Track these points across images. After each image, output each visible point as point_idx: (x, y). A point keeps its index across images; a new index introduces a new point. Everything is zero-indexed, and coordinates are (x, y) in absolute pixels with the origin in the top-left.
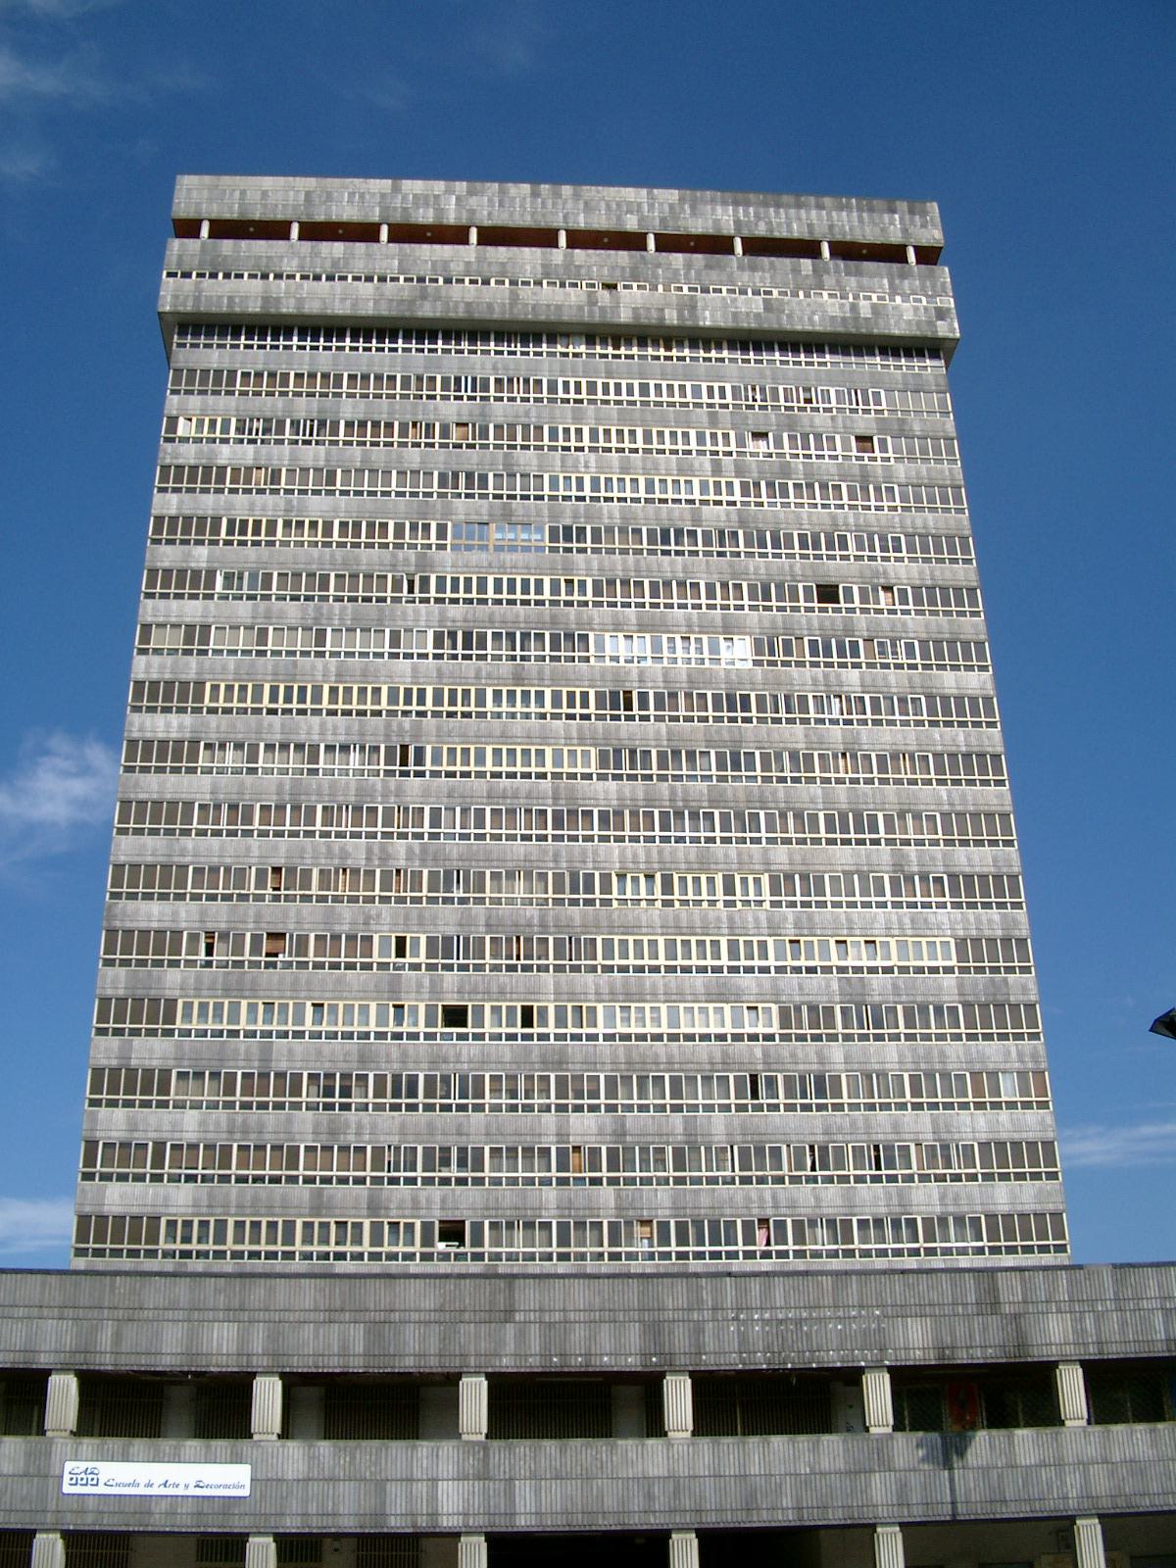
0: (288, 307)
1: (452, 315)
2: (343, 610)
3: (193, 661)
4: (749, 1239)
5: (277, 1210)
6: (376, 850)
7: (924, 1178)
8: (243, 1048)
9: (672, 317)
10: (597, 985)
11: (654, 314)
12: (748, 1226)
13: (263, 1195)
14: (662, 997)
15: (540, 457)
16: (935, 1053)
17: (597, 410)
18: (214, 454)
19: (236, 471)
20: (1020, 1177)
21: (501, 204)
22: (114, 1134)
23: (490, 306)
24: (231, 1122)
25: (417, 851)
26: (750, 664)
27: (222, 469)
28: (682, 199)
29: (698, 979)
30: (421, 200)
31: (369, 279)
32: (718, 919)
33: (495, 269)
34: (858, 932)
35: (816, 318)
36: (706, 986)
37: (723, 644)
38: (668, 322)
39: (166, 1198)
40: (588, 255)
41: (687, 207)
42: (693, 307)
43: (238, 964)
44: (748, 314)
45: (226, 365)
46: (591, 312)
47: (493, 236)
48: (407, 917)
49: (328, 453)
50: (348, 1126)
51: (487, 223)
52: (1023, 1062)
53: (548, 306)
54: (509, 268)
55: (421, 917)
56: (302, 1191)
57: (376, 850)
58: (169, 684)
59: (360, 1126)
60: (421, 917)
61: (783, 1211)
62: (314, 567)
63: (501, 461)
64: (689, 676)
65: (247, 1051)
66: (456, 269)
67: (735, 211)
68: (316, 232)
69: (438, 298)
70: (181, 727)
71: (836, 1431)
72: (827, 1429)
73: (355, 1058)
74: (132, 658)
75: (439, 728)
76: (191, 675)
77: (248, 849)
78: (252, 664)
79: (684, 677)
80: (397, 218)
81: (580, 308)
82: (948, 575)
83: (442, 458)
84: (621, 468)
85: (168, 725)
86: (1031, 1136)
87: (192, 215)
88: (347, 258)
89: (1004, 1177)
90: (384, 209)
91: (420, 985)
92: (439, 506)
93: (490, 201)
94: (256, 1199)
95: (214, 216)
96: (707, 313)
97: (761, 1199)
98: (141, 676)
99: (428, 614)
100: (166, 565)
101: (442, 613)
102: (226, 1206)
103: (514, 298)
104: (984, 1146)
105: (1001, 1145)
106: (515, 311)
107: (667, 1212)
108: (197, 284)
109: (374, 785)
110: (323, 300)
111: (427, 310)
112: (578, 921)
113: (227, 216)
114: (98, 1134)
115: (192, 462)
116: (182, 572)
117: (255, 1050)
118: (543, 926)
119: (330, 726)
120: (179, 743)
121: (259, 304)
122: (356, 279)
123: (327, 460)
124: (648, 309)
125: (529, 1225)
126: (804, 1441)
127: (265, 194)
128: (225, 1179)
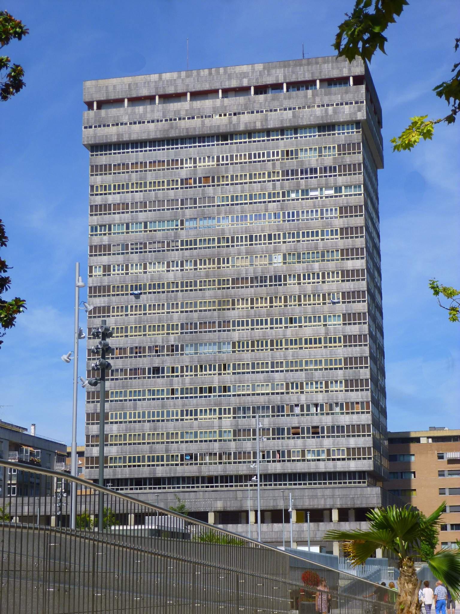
0: (126, 138)
1: (182, 134)
2: (152, 255)
3: (106, 278)
4: (274, 456)
5: (140, 453)
6: (165, 338)
7: (328, 437)
8: (128, 405)
9: (259, 126)
10: (231, 379)
11: (252, 125)
12: (274, 453)
13: (136, 448)
14: (250, 382)
15: (214, 189)
16: (334, 396)
17: (234, 167)
18: (107, 200)
19: (114, 205)
20: (359, 436)
21: (198, 81)
22: (94, 433)
23: (195, 128)
24: (126, 427)
25: (177, 338)
26: (282, 264)
27: (110, 205)
28: (264, 68)
29: (261, 376)
30: (172, 82)
31: (153, 122)
32: (268, 355)
33: (196, 112)
34: (312, 357)
35: (312, 118)
36: (264, 378)
37: (274, 257)
38: (257, 128)
39: (109, 451)
40: (229, 101)
41: (266, 71)
42: (266, 120)
43: (126, 379)
44: (286, 119)
45: (108, 163)
46: (230, 127)
47: (197, 95)
48: (174, 360)
49: (144, 196)
50: (159, 427)
51: (193, 90)
52: (362, 398)
53: (215, 126)
54: (201, 111)
55: (178, 360)
56: (147, 447)
57: (165, 338)
58: (100, 287)
59: (162, 426)
60: (178, 360)
61: (284, 448)
62: (142, 240)
63: (201, 193)
64: (262, 270)
65: (130, 406)
66: (183, 114)
67: (284, 70)
68: (135, 101)
69: (177, 128)
70: (104, 302)
71: (241, 523)
72: (238, 523)
73: (160, 406)
74: (87, 279)
75: (183, 296)
76: (106, 284)
77: (127, 341)
78: (125, 278)
79: (260, 271)
80: (161, 92)
81: (226, 125)
82: (353, 222)
83: (181, 194)
84: (241, 191)
85: (100, 301)
86: (363, 423)
87: (91, 100)
88: (145, 112)
89: (354, 436)
90: (157, 88)
91: (178, 382)
92: (181, 213)
93: (194, 79)
94: (134, 450)
95: (98, 99)
96: (271, 122)
97: (278, 444)
98: (91, 285)
99: (179, 254)
100: (95, 244)
101: (183, 254)
102: (126, 452)
103: (203, 123)
104: (348, 426)
105: (353, 426)
106: (203, 130)
107: (250, 449)
108: (95, 130)
109: (163, 317)
110: (137, 133)
111: (173, 134)
112: (225, 359)
113: (102, 99)
114: (90, 433)
115: (100, 203)
116: (100, 246)
117: (132, 405)
118: (215, 360)
119: (149, 298)
120: (104, 307)
121: (116, 137)
122: (148, 122)
123: (144, 198)
124: (251, 123)
125: (210, 454)
126: (235, 525)
127: (114, 86)
128: (125, 444)
